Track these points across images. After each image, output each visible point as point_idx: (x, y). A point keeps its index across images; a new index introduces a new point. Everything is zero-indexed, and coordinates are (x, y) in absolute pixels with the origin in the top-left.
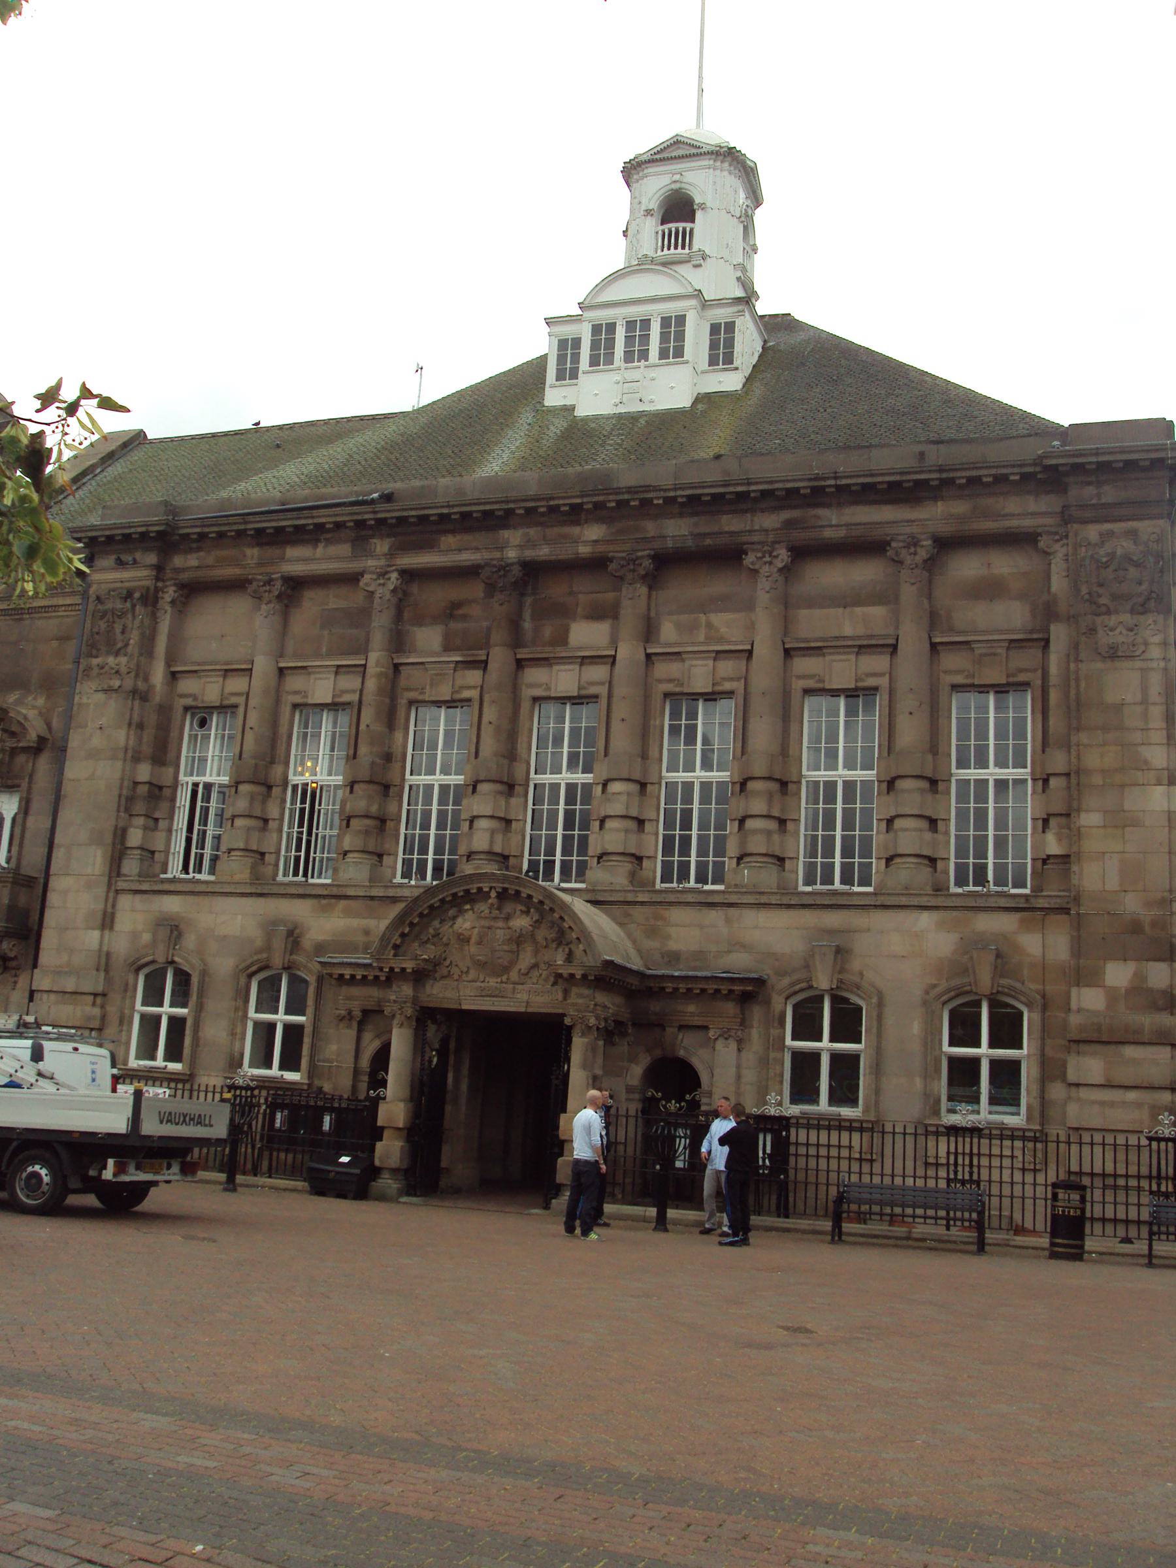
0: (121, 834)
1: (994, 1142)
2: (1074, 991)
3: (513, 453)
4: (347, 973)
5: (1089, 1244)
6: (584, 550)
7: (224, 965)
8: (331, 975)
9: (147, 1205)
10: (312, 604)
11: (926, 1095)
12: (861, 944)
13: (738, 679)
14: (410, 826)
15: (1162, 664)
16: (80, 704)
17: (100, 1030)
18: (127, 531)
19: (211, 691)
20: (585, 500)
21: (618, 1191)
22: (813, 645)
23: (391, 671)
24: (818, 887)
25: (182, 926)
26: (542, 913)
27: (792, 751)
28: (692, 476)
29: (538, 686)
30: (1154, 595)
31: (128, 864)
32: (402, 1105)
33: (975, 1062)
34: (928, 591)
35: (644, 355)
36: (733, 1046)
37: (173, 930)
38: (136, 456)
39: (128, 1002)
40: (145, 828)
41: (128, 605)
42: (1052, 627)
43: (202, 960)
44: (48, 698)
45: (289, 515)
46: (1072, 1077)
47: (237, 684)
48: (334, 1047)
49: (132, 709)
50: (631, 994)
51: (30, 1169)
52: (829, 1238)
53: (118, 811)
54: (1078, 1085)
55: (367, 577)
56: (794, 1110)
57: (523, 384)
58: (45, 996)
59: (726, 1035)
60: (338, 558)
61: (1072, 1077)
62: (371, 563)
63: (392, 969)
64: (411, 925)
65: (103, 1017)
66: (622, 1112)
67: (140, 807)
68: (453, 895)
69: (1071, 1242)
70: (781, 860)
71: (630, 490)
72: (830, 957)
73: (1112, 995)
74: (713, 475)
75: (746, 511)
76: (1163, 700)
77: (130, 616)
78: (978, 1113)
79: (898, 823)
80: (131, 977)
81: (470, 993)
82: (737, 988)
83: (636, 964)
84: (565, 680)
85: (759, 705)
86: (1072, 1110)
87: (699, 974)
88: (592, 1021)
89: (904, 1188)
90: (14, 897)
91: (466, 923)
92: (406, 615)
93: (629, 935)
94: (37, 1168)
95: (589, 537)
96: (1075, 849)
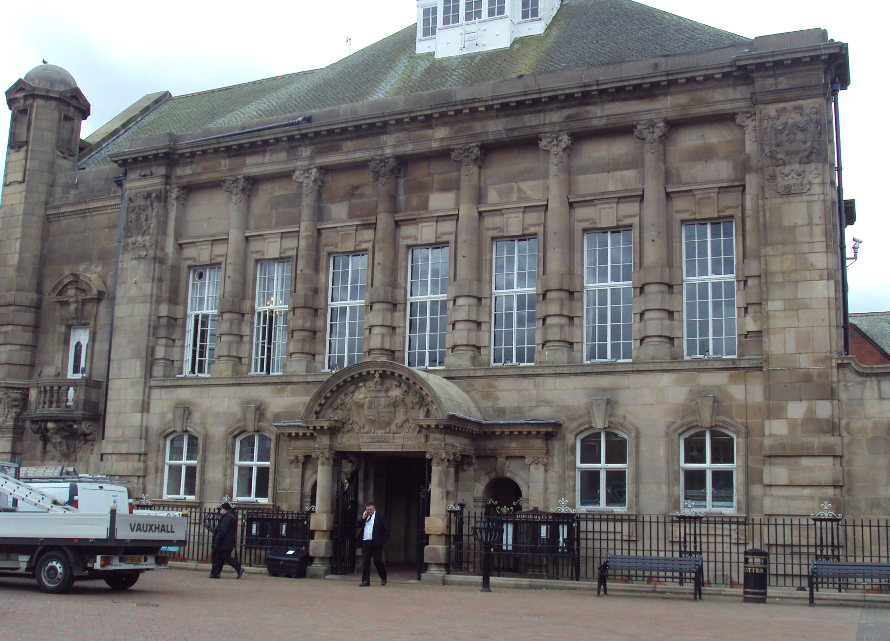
0: (151, 351)
1: (717, 526)
2: (767, 422)
3: (393, 85)
4: (293, 432)
5: (771, 591)
6: (435, 145)
7: (218, 431)
8: (283, 434)
9: (136, 586)
10: (265, 194)
11: (670, 496)
12: (624, 398)
13: (540, 225)
14: (333, 335)
15: (822, 197)
16: (122, 268)
17: (144, 477)
18: (145, 154)
19: (204, 255)
20: (434, 111)
21: (471, 566)
22: (588, 198)
23: (316, 233)
24: (597, 360)
25: (191, 408)
26: (409, 386)
27: (577, 271)
28: (505, 90)
29: (410, 237)
30: (815, 150)
31: (156, 370)
32: (325, 515)
33: (702, 473)
34: (663, 157)
35: (478, 14)
36: (541, 468)
37: (186, 410)
38: (164, 108)
39: (160, 457)
40: (167, 346)
41: (149, 202)
42: (747, 177)
43: (205, 429)
44: (103, 267)
45: (245, 136)
46: (766, 480)
47: (219, 249)
48: (288, 481)
49: (154, 270)
50: (473, 437)
51: (50, 564)
52: (596, 593)
53: (149, 335)
54: (770, 486)
55: (297, 173)
56: (584, 509)
57: (404, 41)
58: (109, 457)
59: (536, 462)
60: (278, 162)
61: (766, 480)
62: (300, 164)
63: (315, 427)
64: (326, 398)
65: (146, 469)
66: (472, 514)
67: (162, 332)
68: (351, 379)
69: (757, 591)
70: (571, 344)
71: (463, 102)
72: (603, 406)
73: (792, 425)
74: (518, 88)
75: (540, 112)
76: (823, 222)
77: (150, 209)
78: (705, 507)
79: (647, 315)
80: (161, 442)
81: (364, 440)
82: (543, 430)
83: (476, 416)
84: (427, 232)
85: (552, 241)
86: (767, 502)
87: (516, 422)
88: (444, 455)
89: (658, 558)
90: (87, 394)
91: (361, 395)
92: (324, 196)
93: (472, 398)
94: (54, 563)
95: (438, 137)
96: (765, 326)
